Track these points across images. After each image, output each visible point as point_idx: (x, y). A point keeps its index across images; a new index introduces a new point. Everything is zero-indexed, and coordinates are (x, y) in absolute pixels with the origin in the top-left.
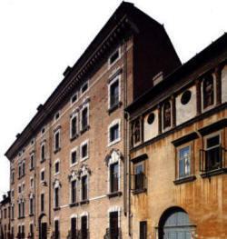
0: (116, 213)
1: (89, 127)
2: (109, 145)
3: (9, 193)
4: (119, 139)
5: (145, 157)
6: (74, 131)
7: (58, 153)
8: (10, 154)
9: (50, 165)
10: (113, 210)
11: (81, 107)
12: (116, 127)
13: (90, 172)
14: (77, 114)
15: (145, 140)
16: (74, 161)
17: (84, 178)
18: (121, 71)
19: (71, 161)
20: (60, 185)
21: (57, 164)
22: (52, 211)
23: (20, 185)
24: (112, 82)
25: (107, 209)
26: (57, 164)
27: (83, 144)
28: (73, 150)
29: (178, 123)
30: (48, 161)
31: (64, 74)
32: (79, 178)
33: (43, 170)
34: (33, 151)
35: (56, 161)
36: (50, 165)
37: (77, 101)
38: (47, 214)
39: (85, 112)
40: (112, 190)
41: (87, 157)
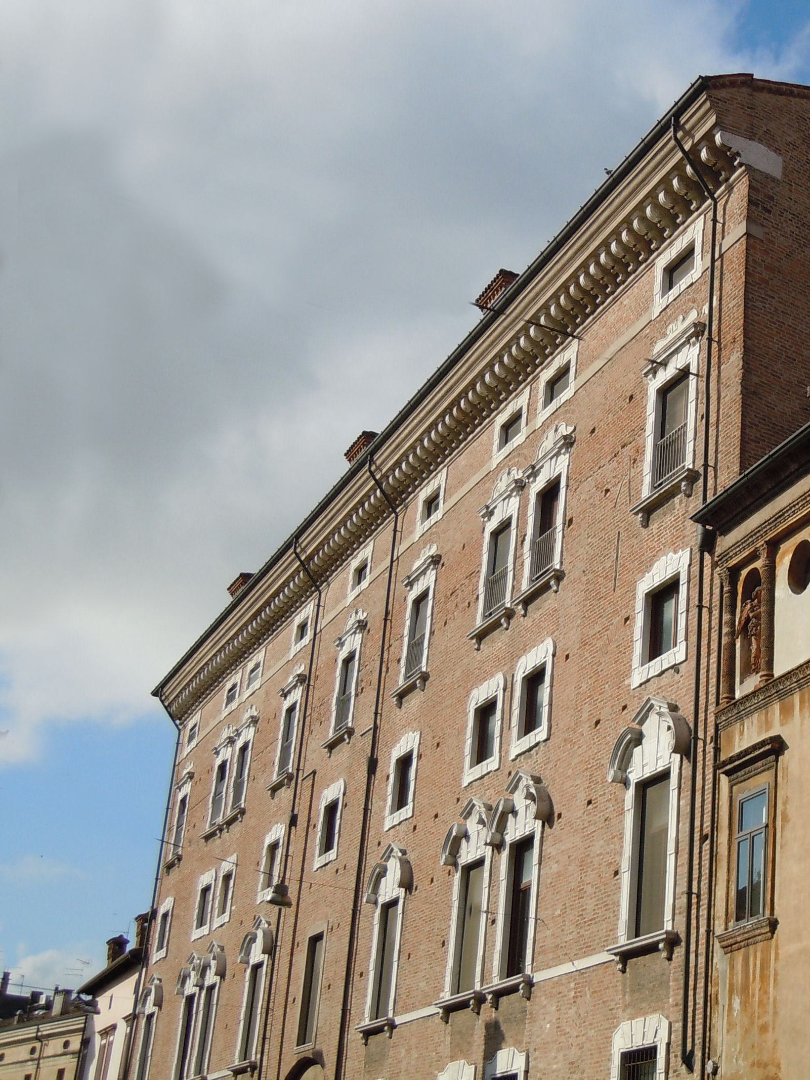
0: (650, 1053)
1: (559, 576)
2: (636, 679)
3: (145, 921)
4: (681, 648)
5: (777, 747)
6: (495, 583)
7: (414, 701)
8: (233, 589)
9: (373, 765)
10: (638, 1043)
11: (534, 473)
12: (669, 588)
13: (547, 817)
14: (514, 503)
15: (778, 672)
16: (482, 752)
17: (523, 846)
18: (699, 330)
19: (638, 647)
20: (407, 884)
21: (404, 762)
22: (354, 1037)
23: (206, 879)
24: (664, 376)
25: (613, 1024)
26: (404, 762)
27: (526, 664)
28: (479, 695)
29: (778, 672)
30: (361, 744)
31: (350, 454)
32: (498, 846)
33: (332, 792)
34: (302, 679)
35: (397, 752)
36: (373, 765)
37: (518, 440)
38: (330, 1059)
39: (549, 495)
40: (457, 988)
41: (540, 733)
